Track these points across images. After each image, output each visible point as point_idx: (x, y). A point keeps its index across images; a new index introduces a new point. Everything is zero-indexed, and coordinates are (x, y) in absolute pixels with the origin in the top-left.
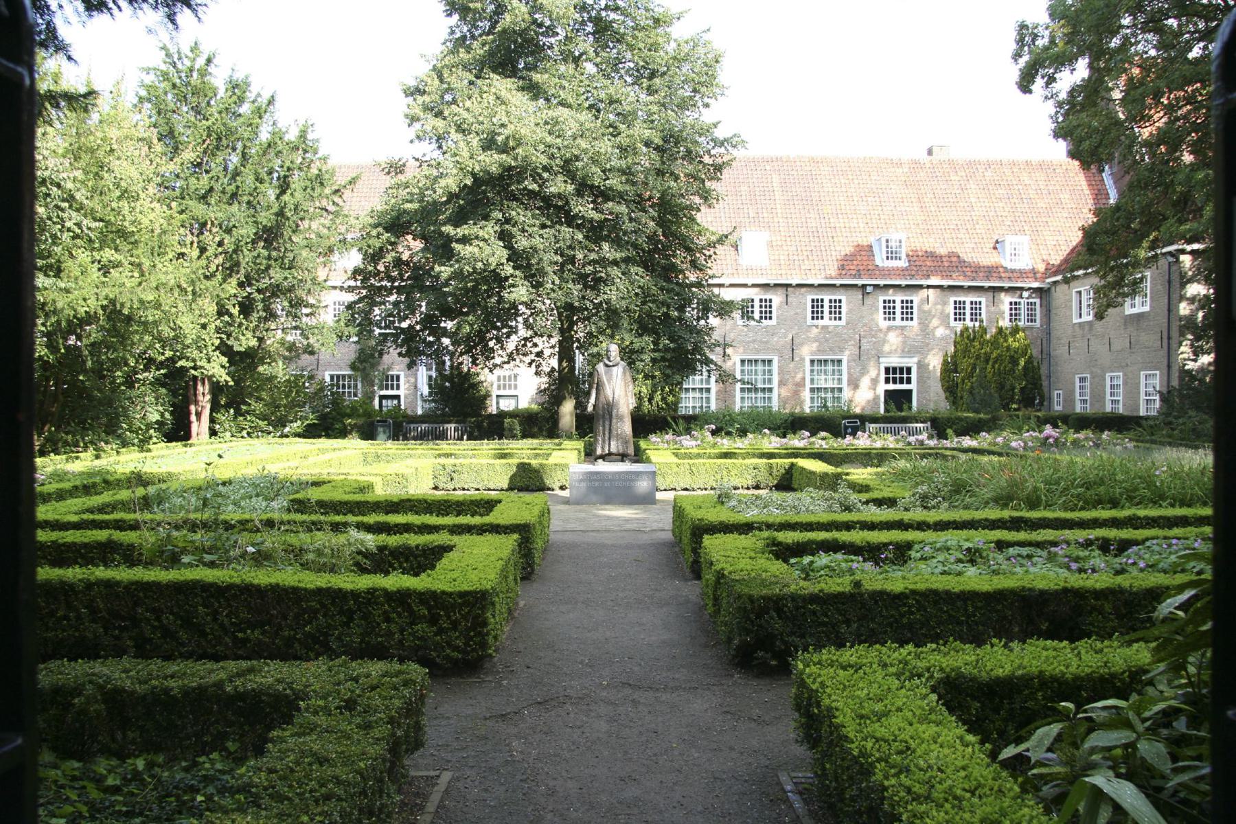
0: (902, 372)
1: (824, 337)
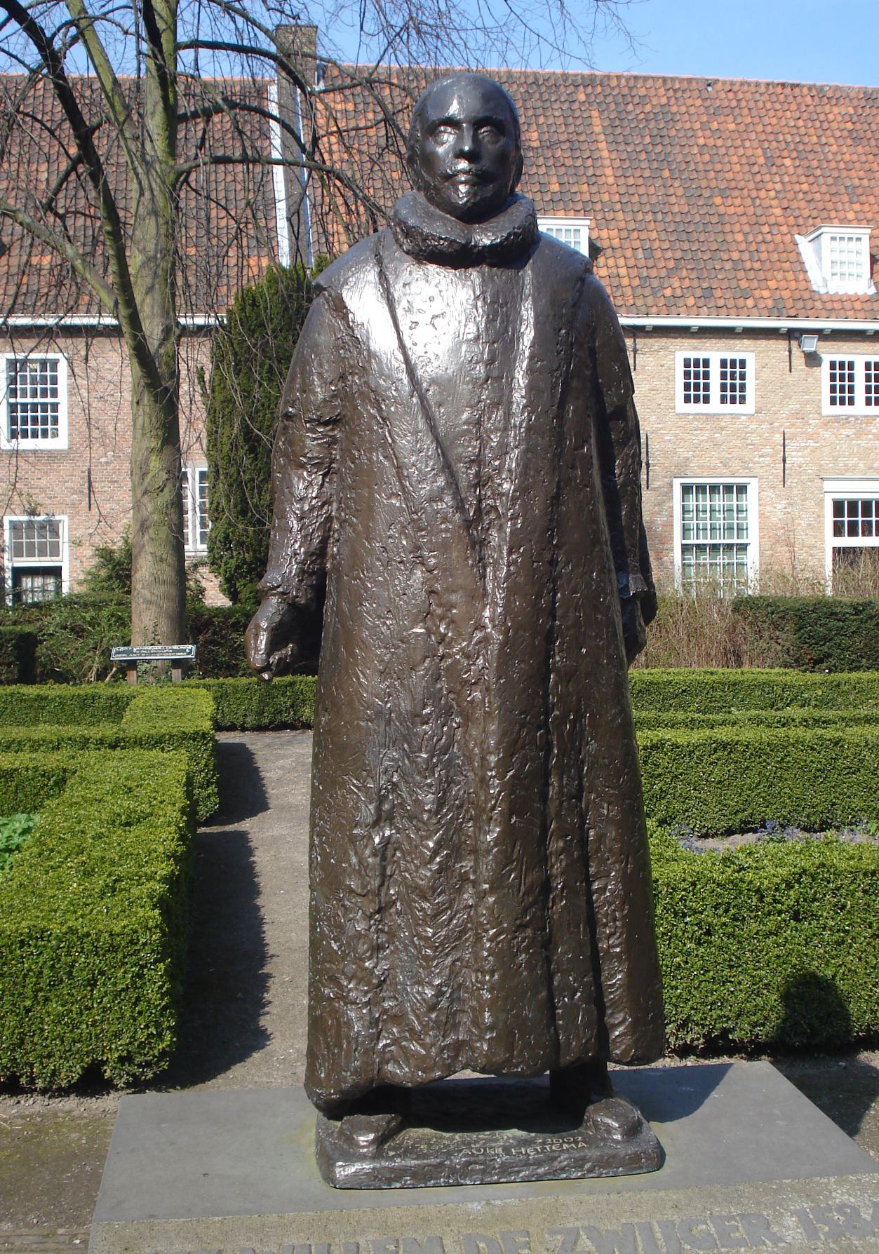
1: (711, 439)
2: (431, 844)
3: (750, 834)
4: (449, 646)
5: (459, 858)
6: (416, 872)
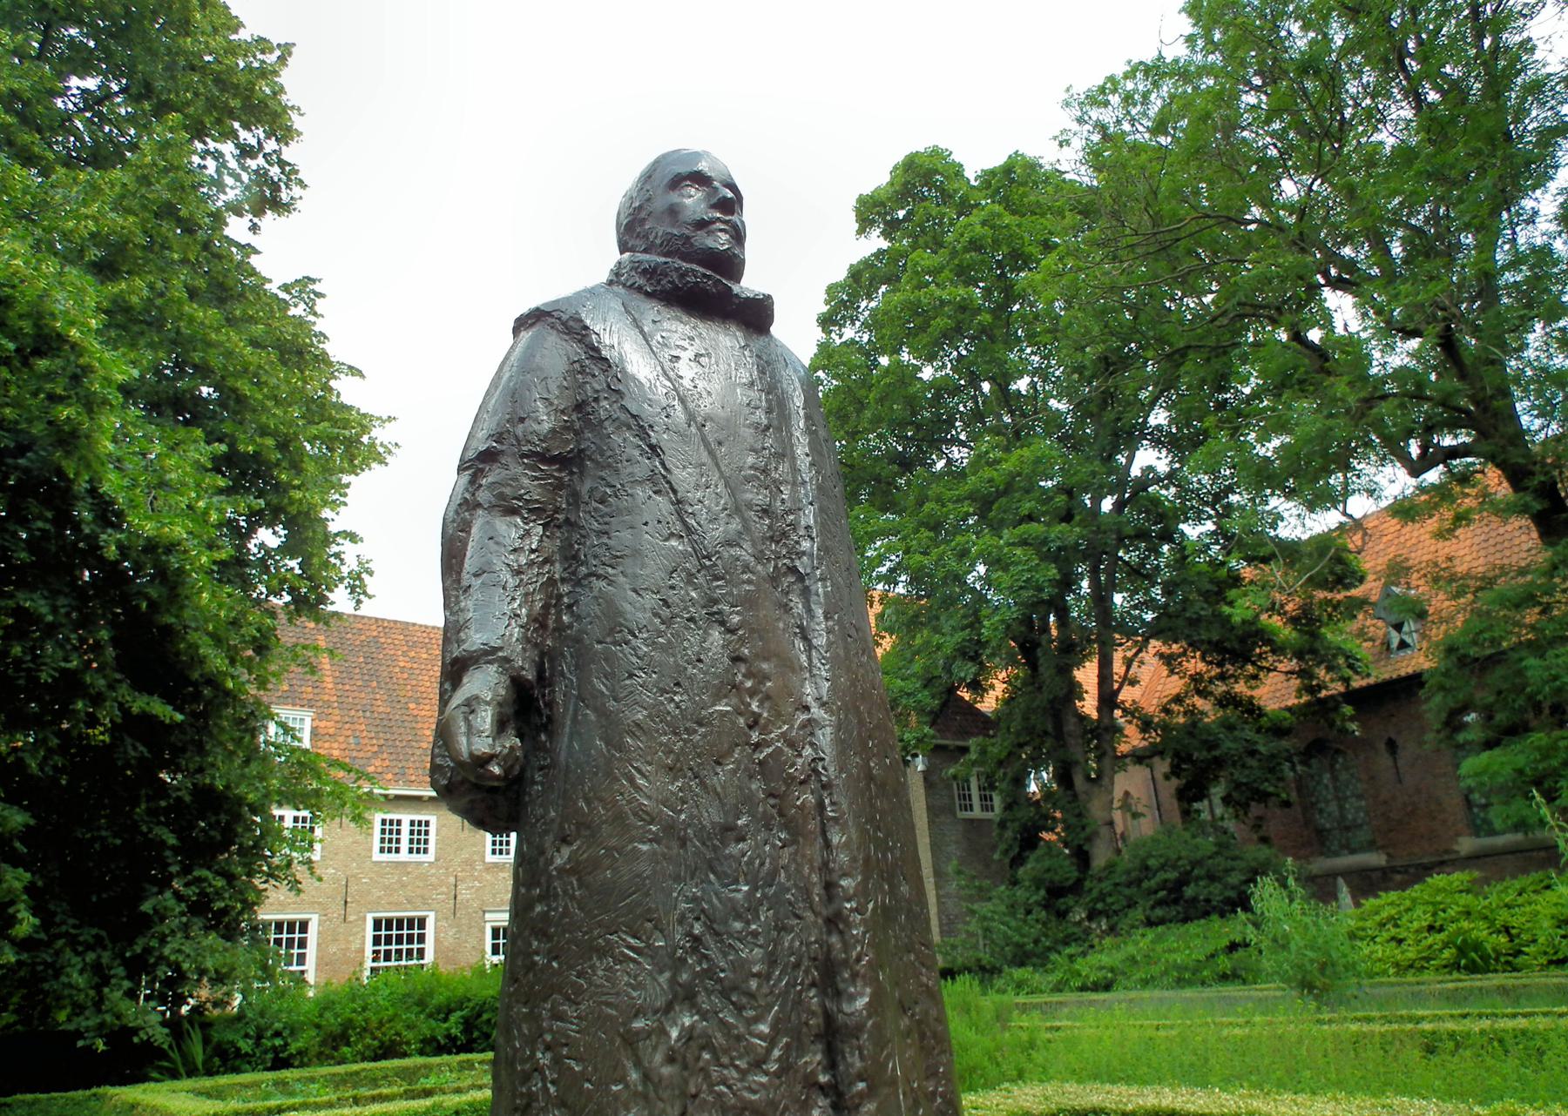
0: (410, 927)
1: (400, 881)
2: (764, 1028)
4: (765, 730)
5: (802, 1051)
6: (742, 1080)
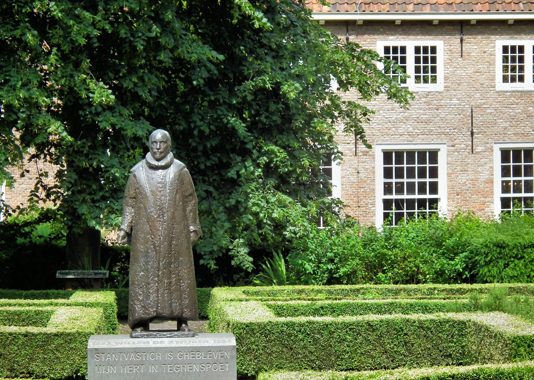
3: (160, 171)
